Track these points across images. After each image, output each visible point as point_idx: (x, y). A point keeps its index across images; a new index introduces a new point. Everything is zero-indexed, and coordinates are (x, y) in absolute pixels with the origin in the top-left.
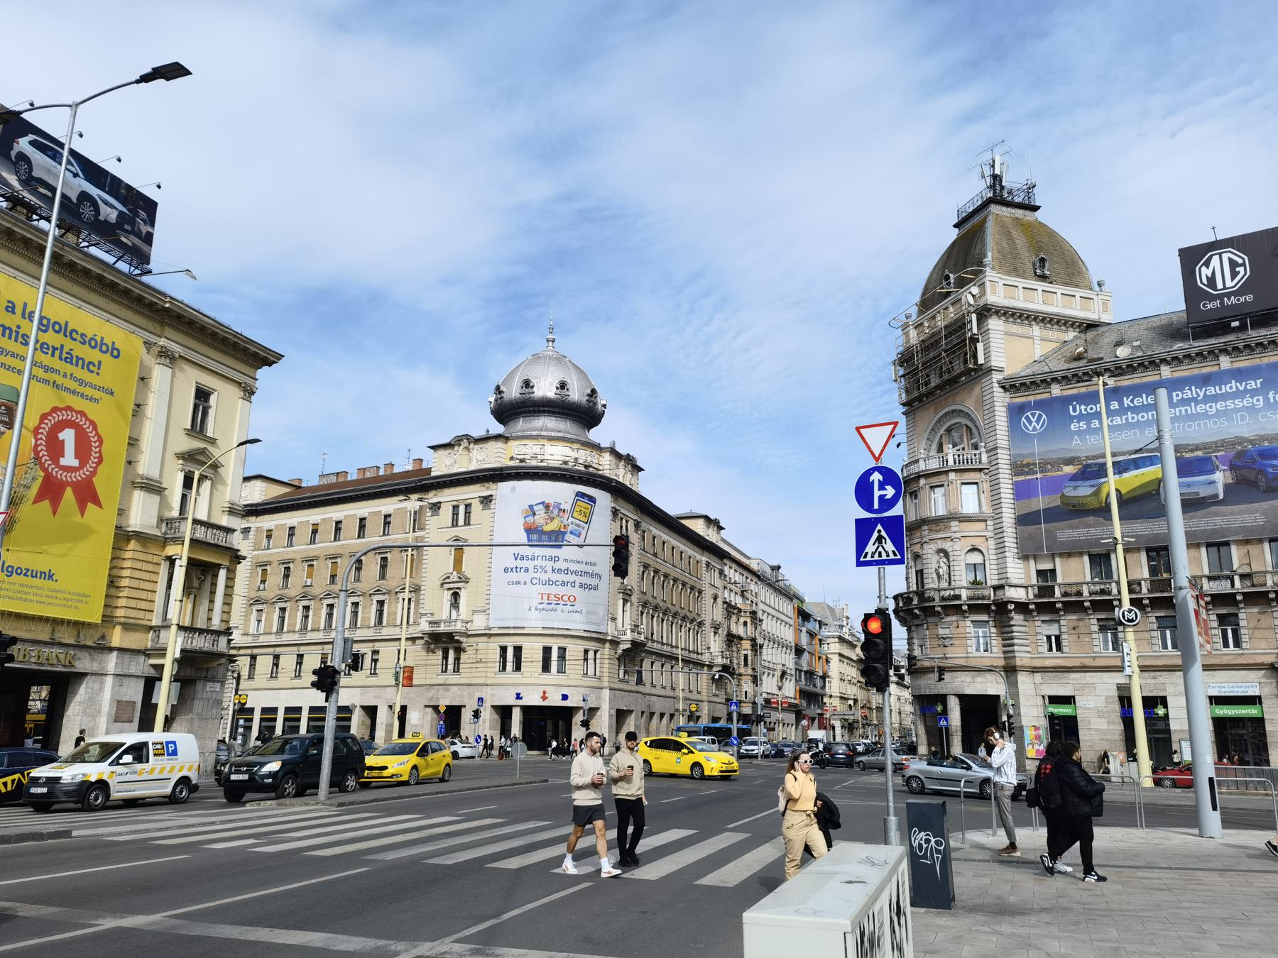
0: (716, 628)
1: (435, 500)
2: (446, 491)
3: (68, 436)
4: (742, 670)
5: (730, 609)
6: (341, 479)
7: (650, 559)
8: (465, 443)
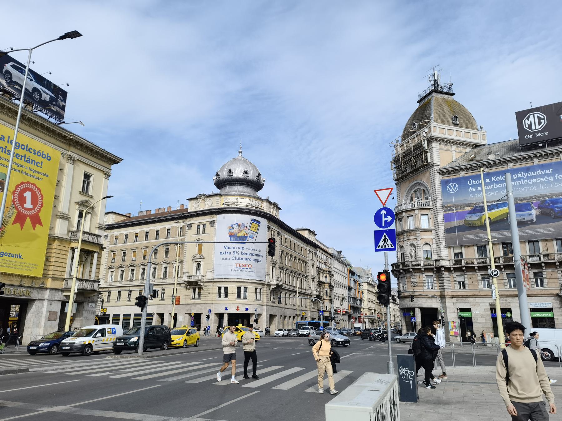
0: (313, 279)
1: (189, 223)
2: (194, 219)
3: (28, 195)
4: (325, 297)
5: (320, 270)
6: (148, 214)
7: (284, 248)
8: (203, 198)
